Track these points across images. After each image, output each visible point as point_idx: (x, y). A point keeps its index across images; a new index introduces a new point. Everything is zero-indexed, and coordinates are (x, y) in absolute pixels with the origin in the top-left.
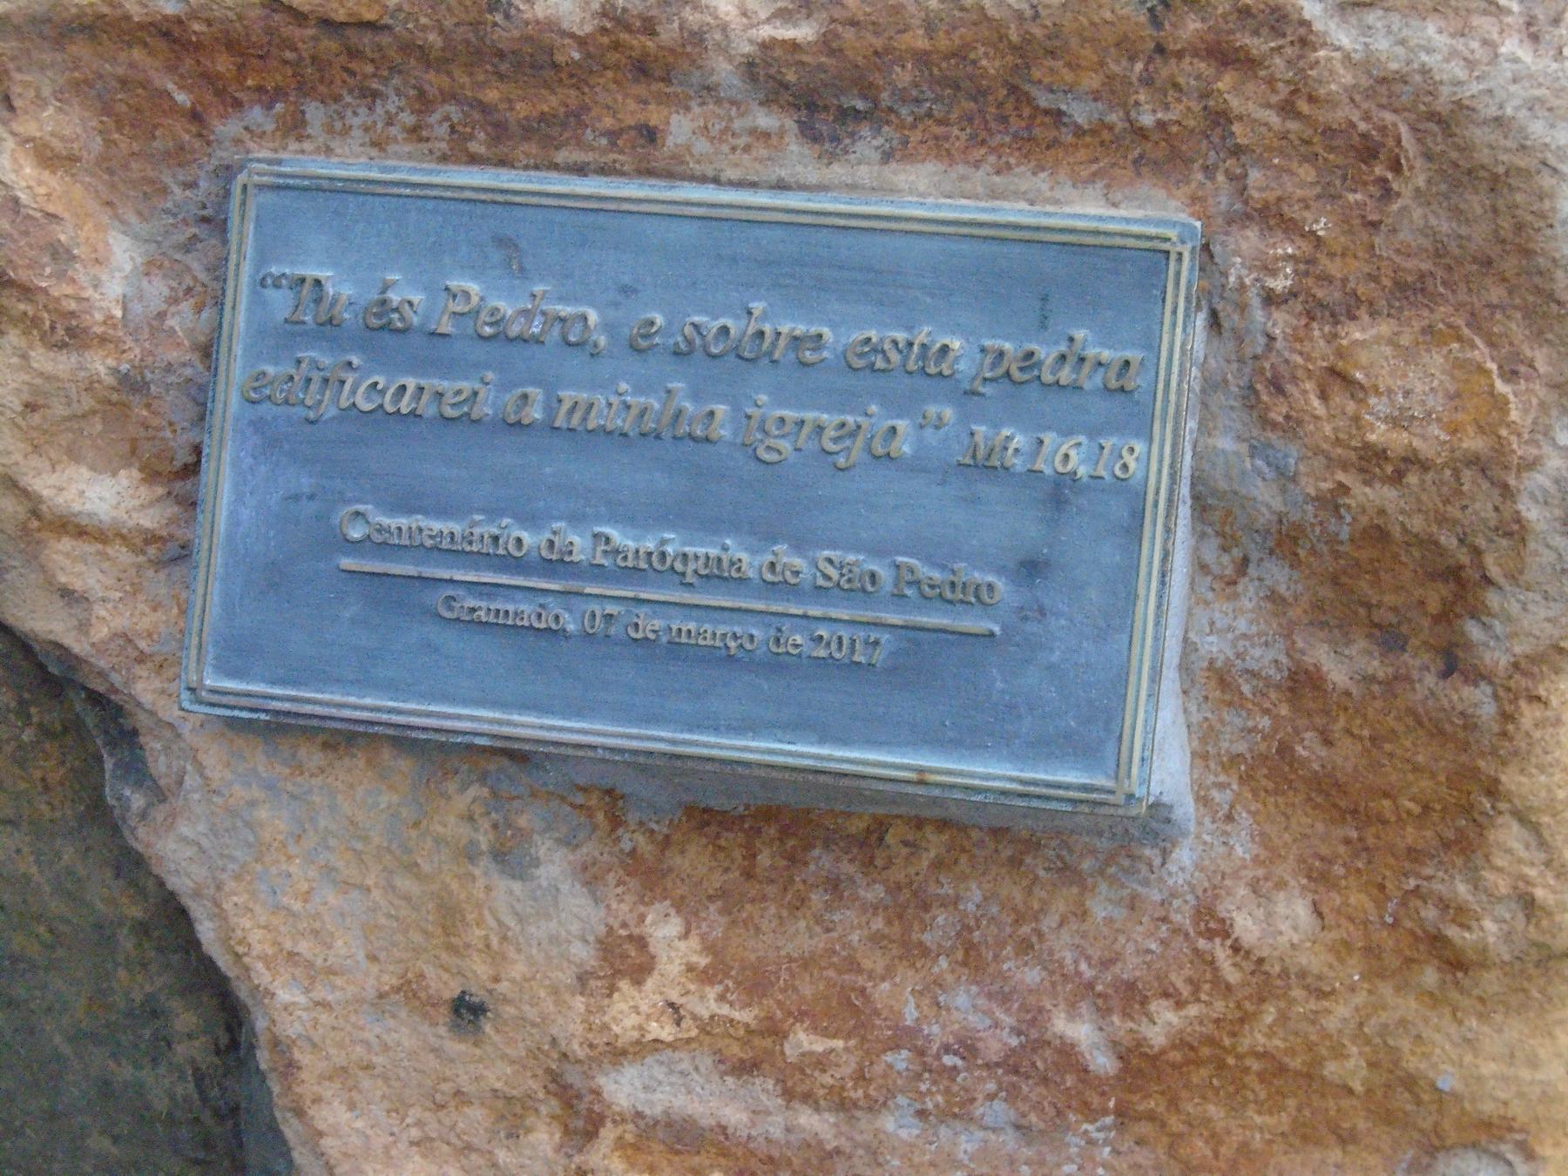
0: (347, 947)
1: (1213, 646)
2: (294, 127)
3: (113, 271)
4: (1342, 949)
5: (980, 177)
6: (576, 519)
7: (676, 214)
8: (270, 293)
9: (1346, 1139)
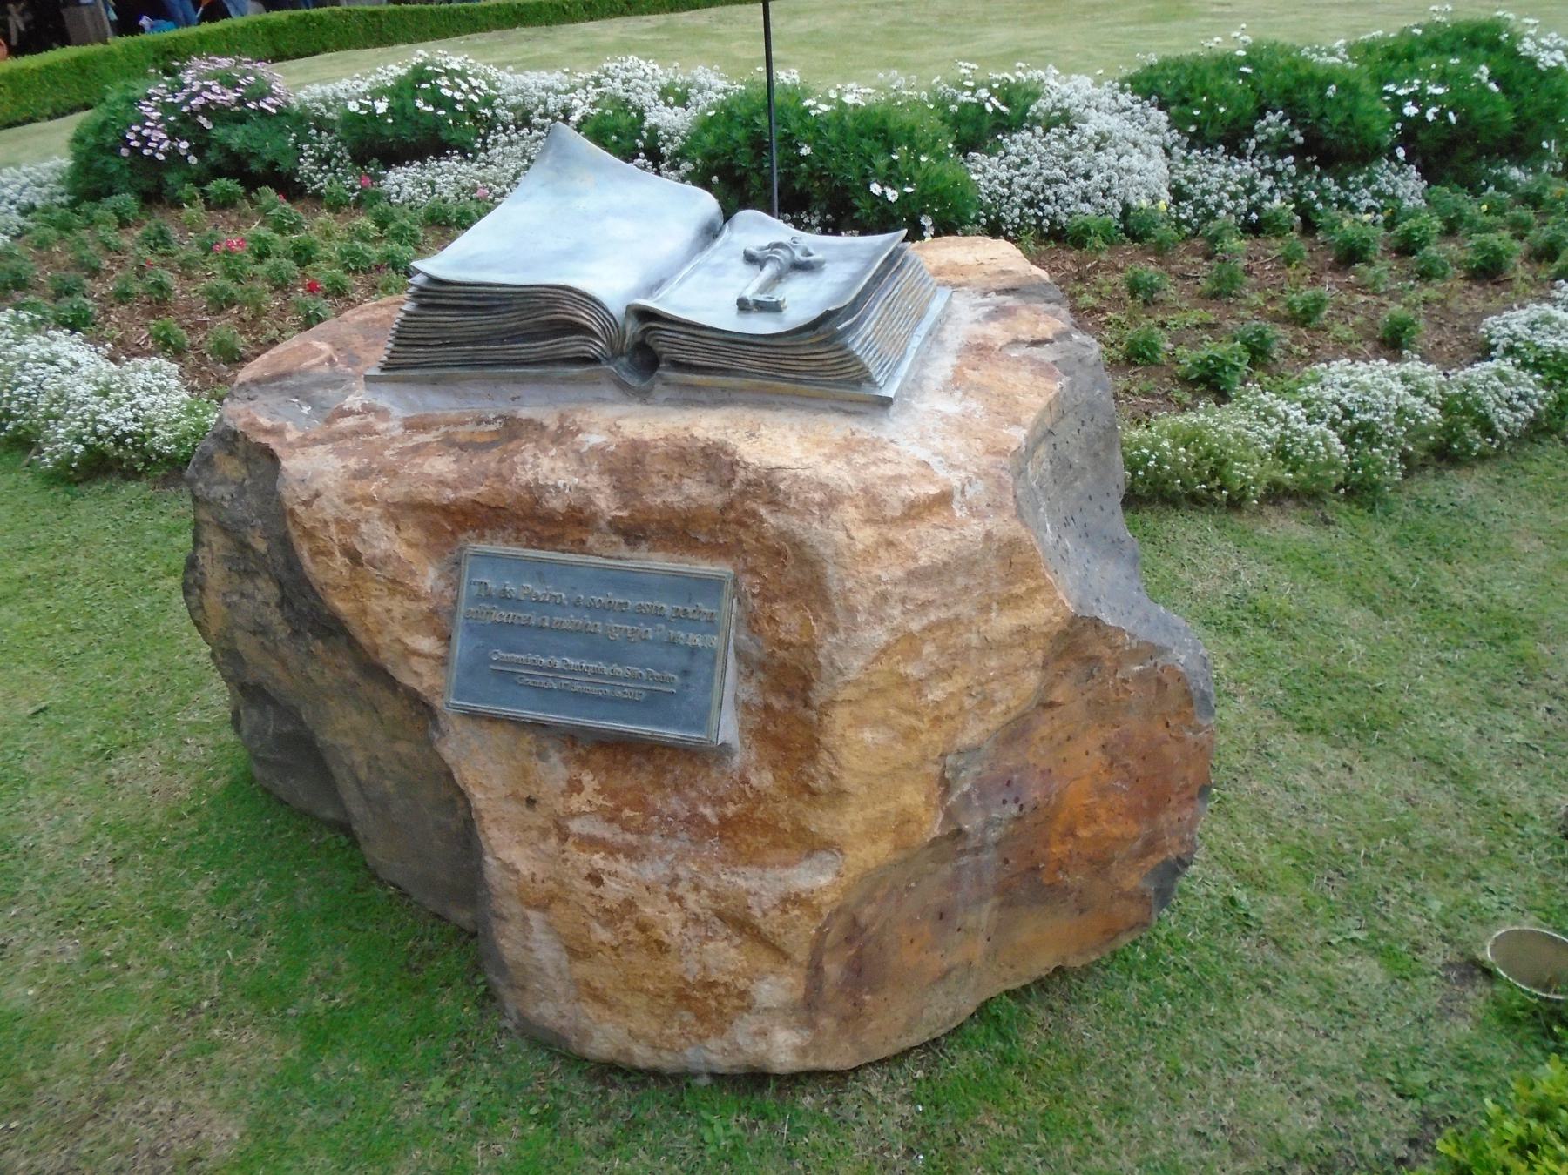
0: (496, 781)
1: (743, 696)
2: (482, 537)
3: (429, 578)
4: (781, 788)
5: (676, 557)
6: (558, 656)
7: (588, 566)
9: (787, 847)
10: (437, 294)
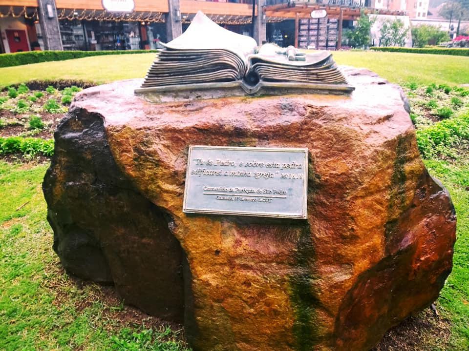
6: (233, 186)
8: (194, 161)
10: (169, 55)
